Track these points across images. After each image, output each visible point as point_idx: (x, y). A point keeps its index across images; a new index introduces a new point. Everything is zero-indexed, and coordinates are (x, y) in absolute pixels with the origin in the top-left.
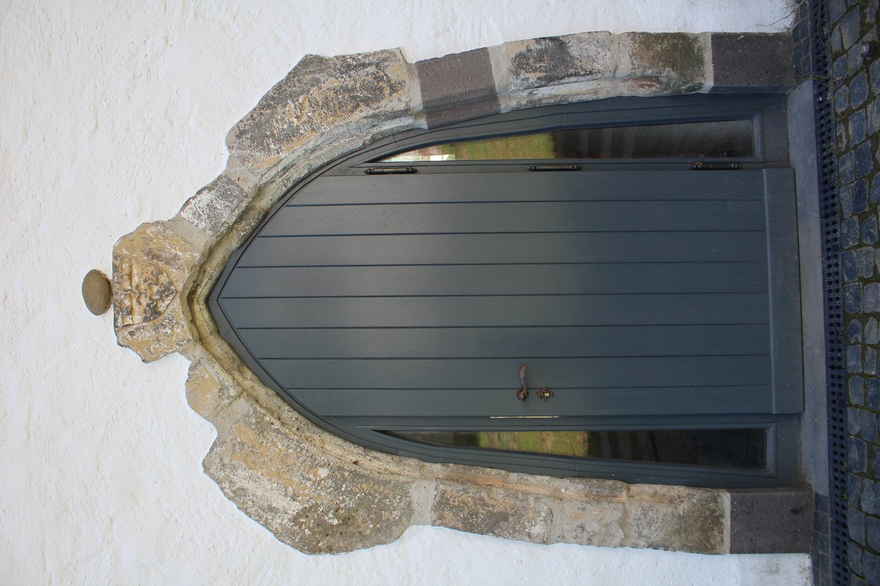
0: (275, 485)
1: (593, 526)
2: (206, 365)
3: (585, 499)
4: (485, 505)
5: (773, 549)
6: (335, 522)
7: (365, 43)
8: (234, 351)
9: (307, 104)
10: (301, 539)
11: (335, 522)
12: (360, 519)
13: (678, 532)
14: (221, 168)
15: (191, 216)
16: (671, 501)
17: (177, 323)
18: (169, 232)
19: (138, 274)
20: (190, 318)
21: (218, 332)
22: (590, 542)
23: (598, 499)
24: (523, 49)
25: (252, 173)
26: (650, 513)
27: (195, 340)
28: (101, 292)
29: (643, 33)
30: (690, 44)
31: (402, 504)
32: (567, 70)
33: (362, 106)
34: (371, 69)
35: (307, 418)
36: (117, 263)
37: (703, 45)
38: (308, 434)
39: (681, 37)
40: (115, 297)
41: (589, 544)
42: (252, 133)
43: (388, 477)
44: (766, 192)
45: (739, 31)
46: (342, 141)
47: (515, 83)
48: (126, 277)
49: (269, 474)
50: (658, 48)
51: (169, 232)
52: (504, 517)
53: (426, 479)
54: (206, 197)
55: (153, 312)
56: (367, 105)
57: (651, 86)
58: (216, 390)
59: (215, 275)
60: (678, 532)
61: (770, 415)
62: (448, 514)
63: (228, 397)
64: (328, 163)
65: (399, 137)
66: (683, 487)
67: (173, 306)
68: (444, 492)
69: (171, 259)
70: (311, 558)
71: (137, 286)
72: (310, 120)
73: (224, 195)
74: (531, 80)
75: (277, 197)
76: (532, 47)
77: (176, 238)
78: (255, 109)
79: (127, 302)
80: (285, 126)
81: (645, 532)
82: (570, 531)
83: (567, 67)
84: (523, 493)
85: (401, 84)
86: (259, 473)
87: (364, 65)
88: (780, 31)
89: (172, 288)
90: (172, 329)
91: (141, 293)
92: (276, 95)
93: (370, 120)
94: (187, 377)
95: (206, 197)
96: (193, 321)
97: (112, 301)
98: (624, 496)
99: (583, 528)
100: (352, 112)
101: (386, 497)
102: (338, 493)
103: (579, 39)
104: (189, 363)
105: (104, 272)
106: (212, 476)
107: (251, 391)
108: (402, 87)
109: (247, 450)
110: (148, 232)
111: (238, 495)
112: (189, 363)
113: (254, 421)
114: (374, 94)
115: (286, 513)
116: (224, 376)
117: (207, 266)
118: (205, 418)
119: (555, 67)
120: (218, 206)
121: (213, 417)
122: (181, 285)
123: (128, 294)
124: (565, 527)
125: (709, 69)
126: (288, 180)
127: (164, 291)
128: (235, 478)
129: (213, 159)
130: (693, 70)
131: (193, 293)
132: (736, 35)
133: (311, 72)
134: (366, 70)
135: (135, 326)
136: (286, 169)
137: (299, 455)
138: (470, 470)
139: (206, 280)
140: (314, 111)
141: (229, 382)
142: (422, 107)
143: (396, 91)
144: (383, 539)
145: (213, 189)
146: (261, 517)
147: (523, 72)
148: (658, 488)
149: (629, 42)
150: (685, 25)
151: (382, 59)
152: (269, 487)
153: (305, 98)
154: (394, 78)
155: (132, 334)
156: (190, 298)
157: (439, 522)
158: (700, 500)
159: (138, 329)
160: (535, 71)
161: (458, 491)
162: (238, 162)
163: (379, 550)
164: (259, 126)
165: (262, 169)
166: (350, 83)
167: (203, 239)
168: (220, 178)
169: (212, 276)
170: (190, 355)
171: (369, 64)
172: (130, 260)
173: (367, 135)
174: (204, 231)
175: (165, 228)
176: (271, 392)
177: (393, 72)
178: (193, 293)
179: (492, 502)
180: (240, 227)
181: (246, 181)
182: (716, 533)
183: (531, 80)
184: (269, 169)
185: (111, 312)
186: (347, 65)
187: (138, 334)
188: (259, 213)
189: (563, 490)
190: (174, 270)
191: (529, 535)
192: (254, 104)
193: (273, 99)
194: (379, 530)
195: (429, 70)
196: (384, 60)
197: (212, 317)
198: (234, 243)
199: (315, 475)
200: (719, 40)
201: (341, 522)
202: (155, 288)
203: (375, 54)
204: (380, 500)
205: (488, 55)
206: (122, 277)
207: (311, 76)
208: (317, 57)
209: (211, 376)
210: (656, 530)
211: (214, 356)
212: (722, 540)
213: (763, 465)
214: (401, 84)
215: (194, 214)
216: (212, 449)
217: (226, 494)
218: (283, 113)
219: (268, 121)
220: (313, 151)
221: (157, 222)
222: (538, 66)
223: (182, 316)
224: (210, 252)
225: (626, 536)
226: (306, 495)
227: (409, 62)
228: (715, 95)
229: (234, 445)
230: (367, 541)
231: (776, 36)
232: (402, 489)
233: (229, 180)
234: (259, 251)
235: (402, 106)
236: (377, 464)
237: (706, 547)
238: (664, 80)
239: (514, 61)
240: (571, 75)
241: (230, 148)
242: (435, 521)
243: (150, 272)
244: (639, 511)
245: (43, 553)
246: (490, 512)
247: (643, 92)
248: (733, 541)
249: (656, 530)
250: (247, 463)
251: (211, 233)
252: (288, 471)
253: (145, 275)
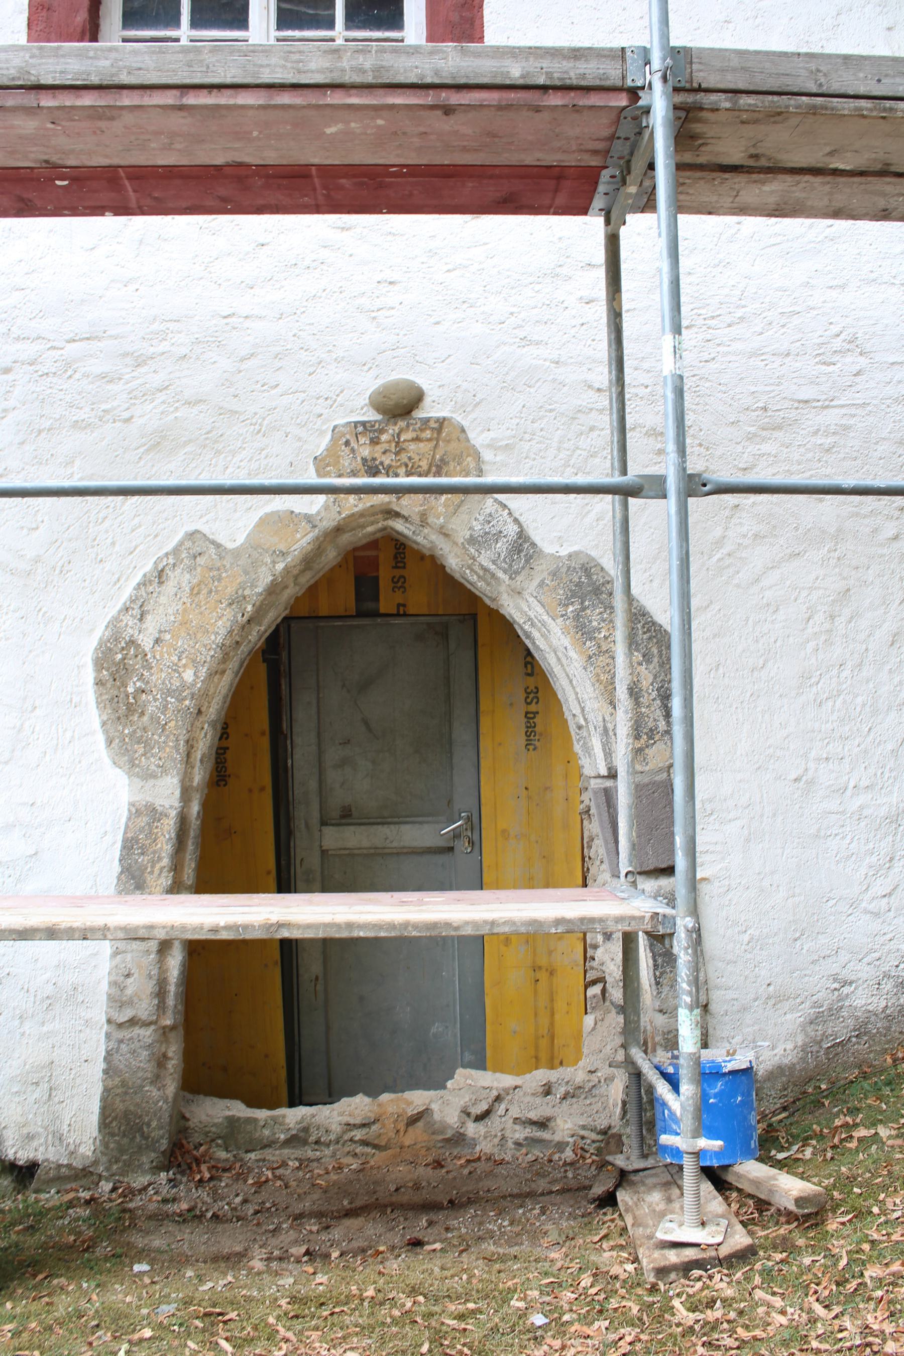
28: (401, 405)
110: (469, 459)
135: (356, 447)
185: (372, 416)
187: (347, 450)
243: (421, 463)
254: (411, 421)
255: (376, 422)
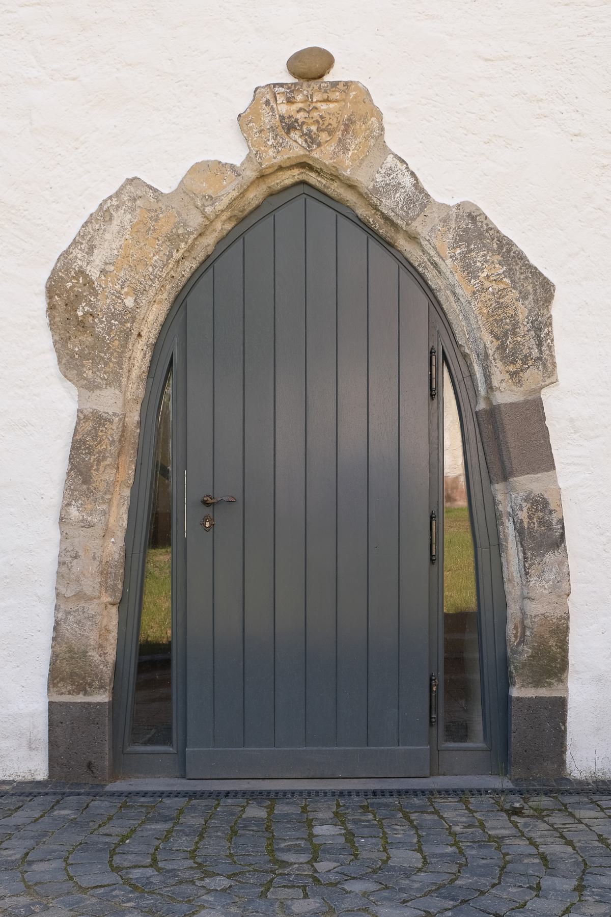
0: (116, 252)
1: (77, 566)
2: (235, 183)
3: (104, 561)
4: (99, 462)
5: (53, 744)
6: (80, 313)
7: (563, 346)
8: (251, 212)
9: (502, 286)
10: (62, 278)
11: (80, 313)
12: (83, 338)
13: (71, 650)
14: (437, 196)
15: (389, 165)
16: (100, 646)
17: (278, 152)
18: (372, 142)
19: (329, 109)
20: (283, 166)
21: (271, 195)
22: (61, 564)
23: (104, 573)
24: (552, 506)
25: (432, 230)
26: (90, 623)
27: (261, 171)
28: (310, 67)
29: (568, 628)
30: (556, 675)
31: (99, 380)
32: (529, 549)
33: (496, 343)
34: (535, 353)
35: (184, 287)
36: (341, 86)
37: (554, 688)
38: (168, 287)
39: (564, 666)
40: (305, 84)
41: (59, 563)
42: (473, 229)
43: (126, 366)
44: (407, 747)
45: (568, 725)
46: (463, 323)
47: (518, 497)
48: (325, 96)
49: (127, 246)
50: (552, 642)
51: (372, 142)
52: (87, 480)
53: (124, 405)
54: (408, 181)
55: (289, 125)
56: (498, 348)
57: (516, 636)
58: (210, 192)
59: (329, 191)
60: (71, 650)
61: (185, 746)
62: (89, 426)
63: (203, 205)
64: (442, 309)
65: (469, 383)
66: (114, 659)
67: (295, 147)
68: (111, 422)
69: (344, 145)
70: (43, 289)
71: (316, 108)
72: (484, 289)
73: (409, 201)
74: (520, 513)
75: (408, 256)
76: (554, 515)
77: (366, 149)
78: (498, 232)
79: (299, 97)
80: (478, 264)
81: (71, 618)
82: (72, 545)
83: (533, 549)
84: (110, 500)
85: (519, 383)
86: (127, 237)
87: (540, 345)
88: (568, 766)
89: (314, 146)
90: (273, 146)
91: (308, 112)
92: (512, 254)
93: (482, 351)
94: (224, 161)
95: (408, 181)
96: (281, 168)
97: (302, 81)
98: (106, 599)
99: (76, 557)
100: (491, 333)
101: (106, 364)
102: (109, 317)
103: (563, 562)
104: (238, 165)
105: (332, 71)
106: (123, 187)
107: (210, 229)
108: (516, 384)
109: (151, 224)
110: (373, 119)
111: (104, 214)
112: (238, 165)
113: (180, 231)
114: (509, 355)
115: (88, 264)
116: (226, 201)
117: (338, 183)
118: (182, 181)
119: (533, 538)
120: (397, 195)
121: (183, 189)
122: (317, 156)
123: (308, 99)
124: (77, 540)
125: (530, 693)
126: (425, 268)
127: (311, 137)
128: (122, 211)
129: (445, 191)
130: (528, 677)
131: (311, 168)
132: (564, 722)
133: (535, 291)
134: (535, 347)
135: (275, 106)
136: (435, 265)
137: (147, 278)
138: (133, 448)
139: (324, 182)
140: (493, 294)
141: (220, 206)
142: (495, 404)
143: (511, 378)
144: (64, 361)
145: (416, 189)
146: (83, 237)
147: (529, 505)
148: (114, 634)
149: (559, 613)
150: (577, 672)
151: (546, 364)
152: (114, 246)
153: (507, 284)
154: (526, 375)
155: (267, 103)
156: (304, 165)
157: (82, 417)
158: (102, 672)
159: (272, 109)
160: (530, 517)
161: (112, 435)
162: (443, 215)
163: (52, 357)
164: (481, 236)
165: (435, 240)
166: (522, 330)
167: (363, 178)
168: (427, 195)
169: (328, 188)
170: (246, 165)
171: (540, 350)
172: (344, 100)
173: (470, 349)
174: (373, 180)
175: (376, 138)
176: (210, 250)
177: (532, 375)
178: (311, 168)
179: (101, 469)
180: (378, 217)
181: (424, 223)
182: (69, 687)
183: (520, 513)
184: (435, 248)
185: (290, 80)
186: (541, 328)
187: (267, 109)
188: (392, 238)
189: (113, 540)
190: (332, 148)
191: (69, 505)
192: (505, 231)
193: (509, 251)
194: (72, 357)
195: (534, 410)
196: (545, 366)
197: (286, 189)
198: (362, 211)
199: (127, 294)
200: (560, 704)
201: (80, 319)
202: (314, 128)
203: (552, 357)
204: (102, 358)
205: (547, 471)
206: (326, 92)
207: (531, 290)
208: (552, 296)
209: (225, 187)
210: (72, 629)
211: (246, 190)
212: (62, 694)
213: (134, 742)
214: (519, 383)
215: (391, 169)
216: (150, 187)
217: (105, 201)
218: (493, 262)
219: (485, 247)
220: (454, 294)
221: (382, 129)
222: (535, 520)
223: (286, 157)
224: (352, 187)
225: (67, 598)
226: (106, 284)
227: (543, 391)
228: (507, 698)
229: (156, 211)
230: (61, 345)
231: (563, 762)
232: (114, 380)
233: (425, 206)
234: (353, 237)
235: (495, 383)
236: (139, 356)
237: (56, 677)
238: (520, 648)
239: (541, 496)
240: (525, 554)
241: (458, 206)
242: (82, 412)
243: (331, 122)
244: (91, 612)
245: (39, 4)
246: (92, 466)
247: (510, 627)
248: (62, 704)
249: (72, 629)
250: (137, 223)
251: (371, 187)
252: (130, 266)
253: (327, 117)
254: (323, 85)
255: (292, 84)
